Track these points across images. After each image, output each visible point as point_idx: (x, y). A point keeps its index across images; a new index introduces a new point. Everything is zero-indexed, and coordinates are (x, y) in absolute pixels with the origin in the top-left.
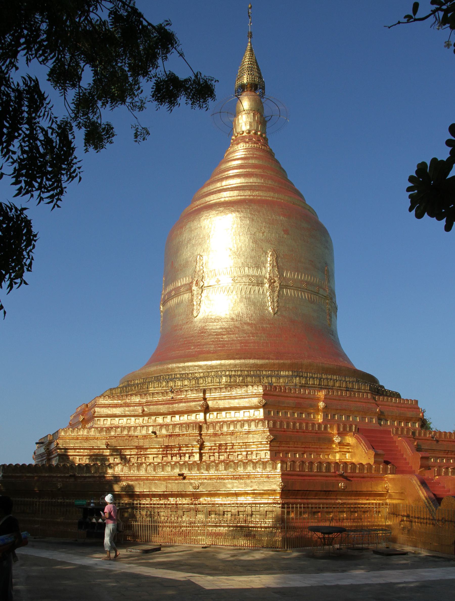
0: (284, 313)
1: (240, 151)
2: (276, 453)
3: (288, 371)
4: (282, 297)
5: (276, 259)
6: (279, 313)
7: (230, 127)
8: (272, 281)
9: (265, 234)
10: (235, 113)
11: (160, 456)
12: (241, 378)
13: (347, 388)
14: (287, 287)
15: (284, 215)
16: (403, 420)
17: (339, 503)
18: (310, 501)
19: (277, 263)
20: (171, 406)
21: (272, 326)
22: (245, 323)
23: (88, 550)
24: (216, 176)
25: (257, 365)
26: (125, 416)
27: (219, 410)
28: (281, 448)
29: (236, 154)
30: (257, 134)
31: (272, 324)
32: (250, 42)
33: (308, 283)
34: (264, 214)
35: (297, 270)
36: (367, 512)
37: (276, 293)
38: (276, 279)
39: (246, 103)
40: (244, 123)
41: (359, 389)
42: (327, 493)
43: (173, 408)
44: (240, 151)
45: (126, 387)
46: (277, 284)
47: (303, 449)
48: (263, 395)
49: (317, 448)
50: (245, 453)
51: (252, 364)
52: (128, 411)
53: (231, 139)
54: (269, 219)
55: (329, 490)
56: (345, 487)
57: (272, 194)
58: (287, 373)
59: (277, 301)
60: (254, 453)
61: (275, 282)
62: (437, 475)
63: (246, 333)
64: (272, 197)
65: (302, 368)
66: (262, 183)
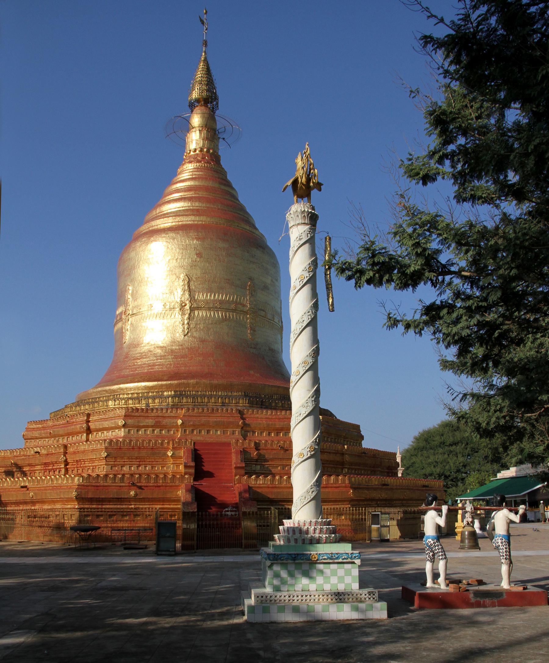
0: (195, 334)
1: (188, 171)
2: (112, 467)
3: (171, 391)
4: (194, 318)
5: (189, 282)
6: (189, 334)
7: (183, 144)
8: (183, 304)
9: (179, 260)
10: (187, 127)
11: (43, 471)
12: (123, 401)
13: (223, 403)
14: (198, 308)
15: (198, 239)
16: (273, 430)
17: (132, 508)
18: (104, 507)
19: (189, 286)
20: (66, 429)
21: (180, 347)
22: (158, 347)
23: (136, 556)
24: (168, 195)
25: (148, 387)
26: (42, 438)
27: (98, 430)
28: (116, 463)
29: (183, 175)
30: (203, 151)
31: (182, 345)
32: (205, 52)
33: (221, 302)
34: (178, 241)
35: (210, 290)
36: (139, 515)
37: (187, 316)
38: (187, 302)
39: (196, 120)
40: (195, 140)
41: (237, 403)
42: (120, 500)
43: (68, 430)
44: (188, 171)
45: (172, 397)
46: (187, 307)
47: (138, 463)
48: (125, 416)
49: (153, 461)
50: (92, 468)
51: (144, 387)
52: (44, 434)
53: (183, 155)
54: (183, 245)
55: (120, 497)
56: (136, 495)
57: (193, 218)
58: (170, 393)
59: (188, 323)
60: (97, 467)
61: (185, 305)
62: (238, 483)
63: (156, 357)
64: (193, 221)
65: (189, 387)
66: (189, 206)
